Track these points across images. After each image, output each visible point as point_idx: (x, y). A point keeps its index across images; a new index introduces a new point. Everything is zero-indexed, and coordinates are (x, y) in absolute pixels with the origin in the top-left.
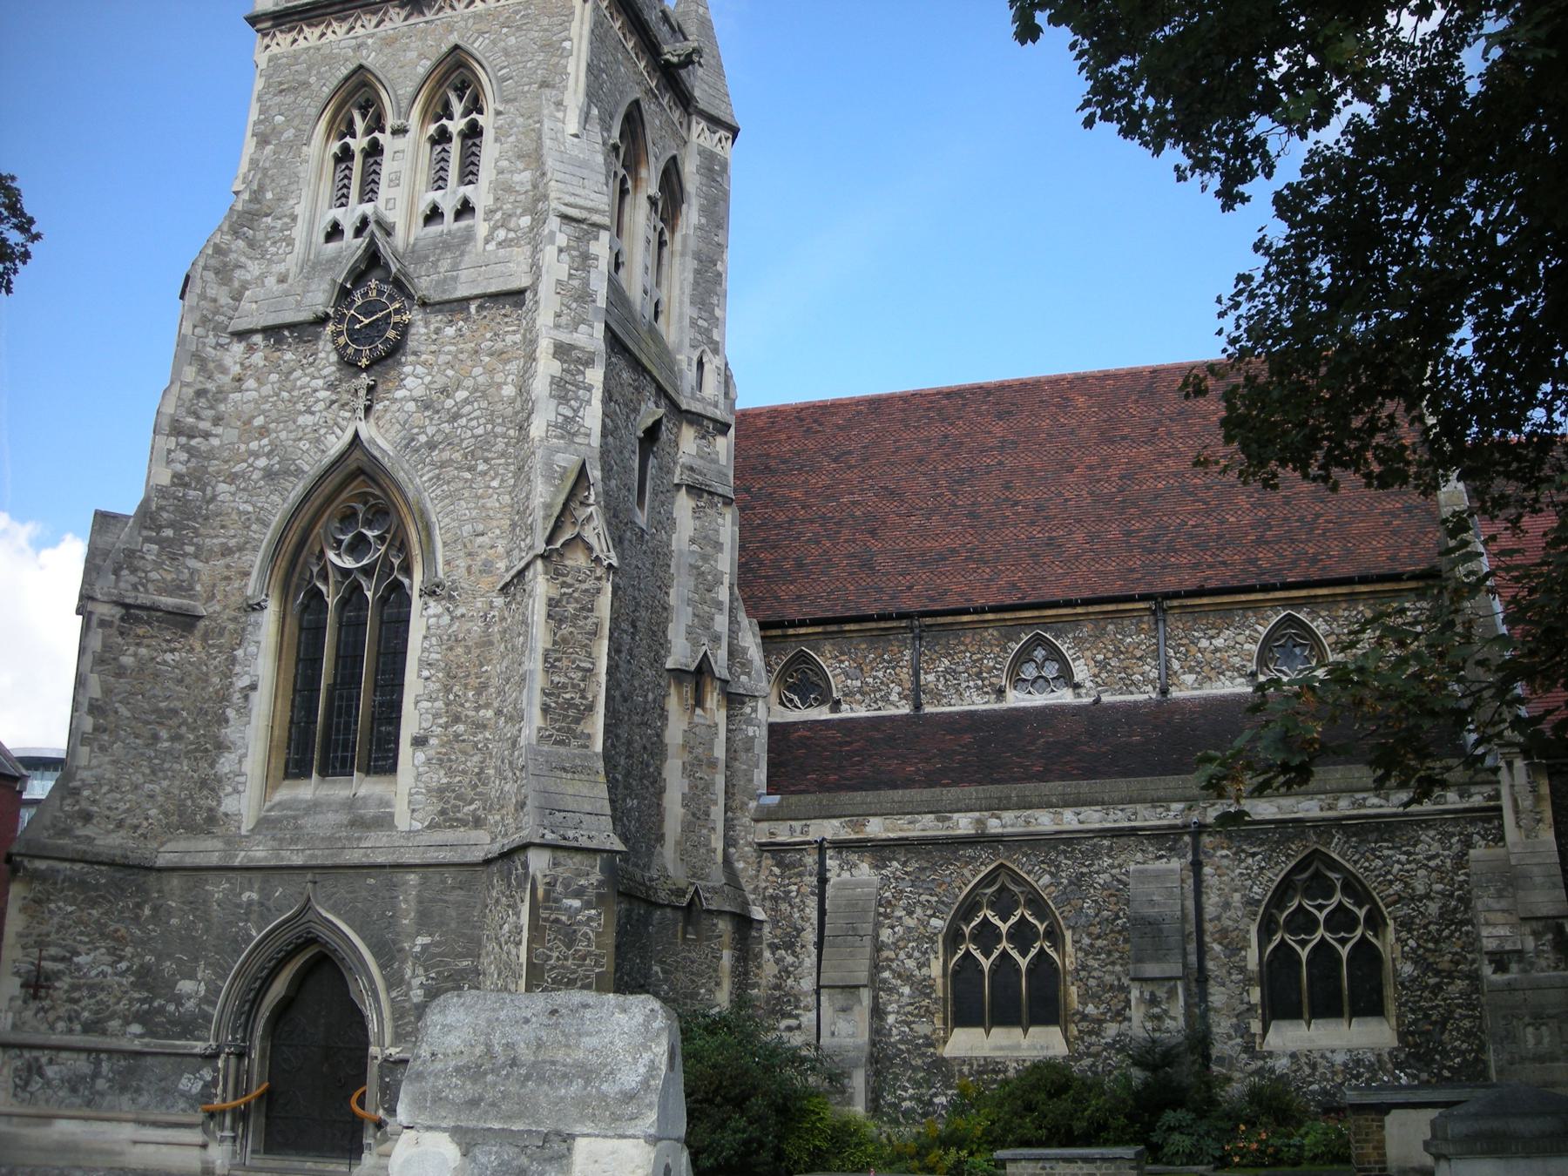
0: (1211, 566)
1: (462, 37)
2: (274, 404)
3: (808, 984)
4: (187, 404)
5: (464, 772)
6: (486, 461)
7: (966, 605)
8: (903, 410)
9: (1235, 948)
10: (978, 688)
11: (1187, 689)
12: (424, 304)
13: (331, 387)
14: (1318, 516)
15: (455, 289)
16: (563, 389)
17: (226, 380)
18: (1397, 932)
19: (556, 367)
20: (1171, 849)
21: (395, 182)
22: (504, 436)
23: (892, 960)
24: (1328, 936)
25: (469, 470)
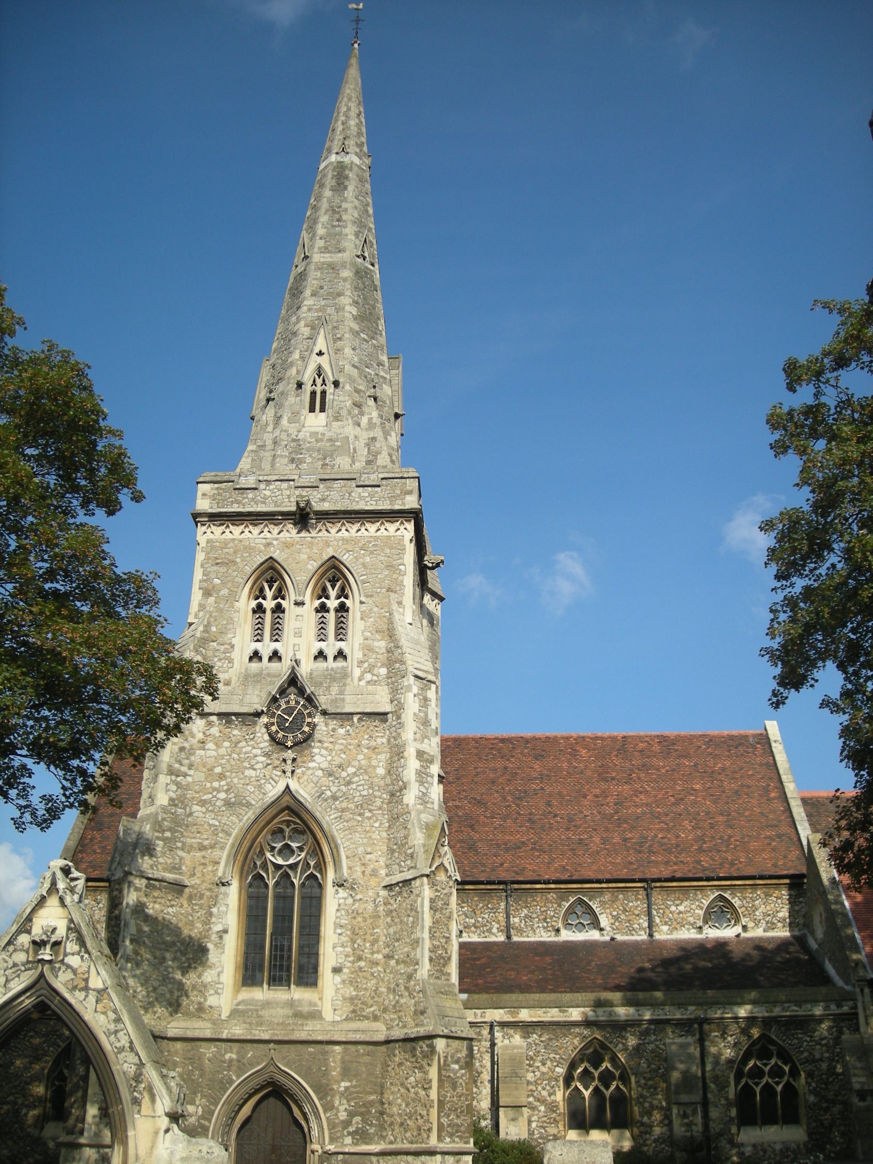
0: (675, 864)
1: (336, 551)
2: (228, 761)
4: (175, 756)
5: (366, 989)
6: (370, 811)
7: (537, 878)
8: (476, 748)
9: (722, 1086)
10: (544, 928)
11: (663, 934)
12: (324, 713)
13: (267, 755)
14: (730, 837)
15: (344, 707)
16: (422, 776)
17: (194, 741)
18: (806, 1078)
20: (687, 1031)
22: (380, 797)
23: (534, 1091)
24: (770, 1080)
25: (360, 815)
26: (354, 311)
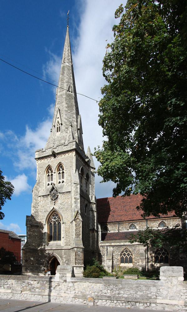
3: (106, 259)
16: (75, 202)
19: (74, 200)
21: (55, 179)
26: (66, 105)
